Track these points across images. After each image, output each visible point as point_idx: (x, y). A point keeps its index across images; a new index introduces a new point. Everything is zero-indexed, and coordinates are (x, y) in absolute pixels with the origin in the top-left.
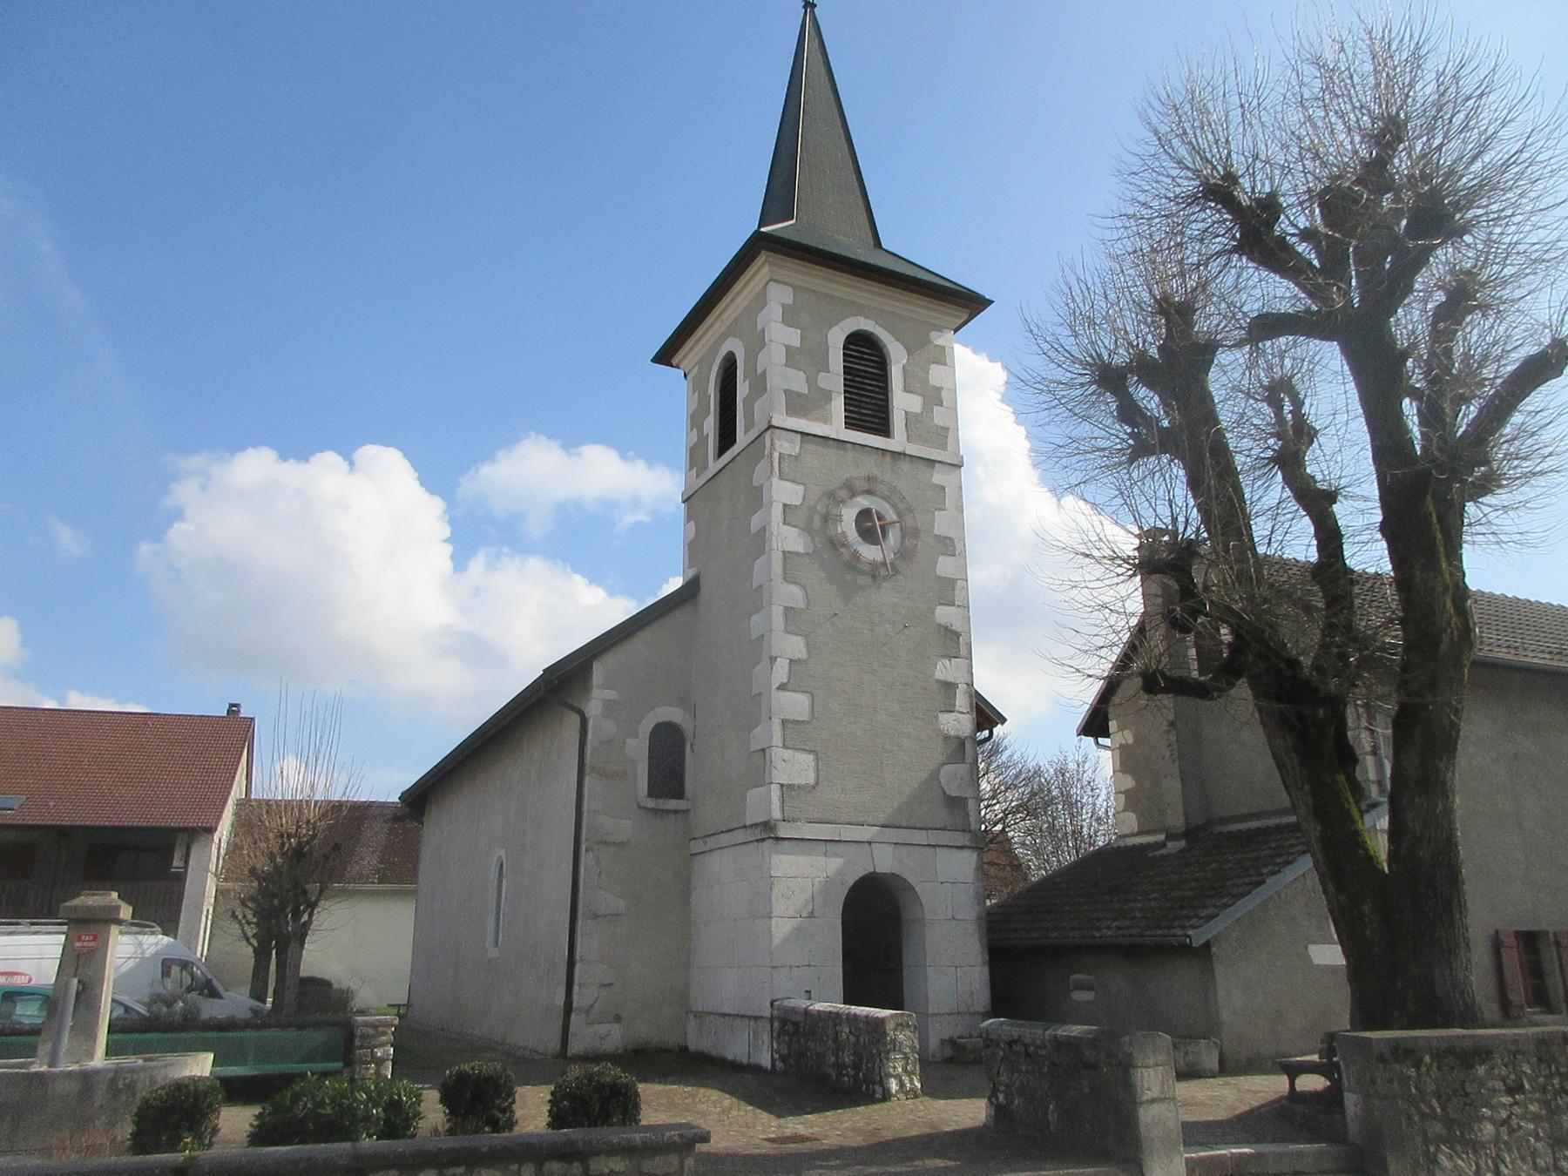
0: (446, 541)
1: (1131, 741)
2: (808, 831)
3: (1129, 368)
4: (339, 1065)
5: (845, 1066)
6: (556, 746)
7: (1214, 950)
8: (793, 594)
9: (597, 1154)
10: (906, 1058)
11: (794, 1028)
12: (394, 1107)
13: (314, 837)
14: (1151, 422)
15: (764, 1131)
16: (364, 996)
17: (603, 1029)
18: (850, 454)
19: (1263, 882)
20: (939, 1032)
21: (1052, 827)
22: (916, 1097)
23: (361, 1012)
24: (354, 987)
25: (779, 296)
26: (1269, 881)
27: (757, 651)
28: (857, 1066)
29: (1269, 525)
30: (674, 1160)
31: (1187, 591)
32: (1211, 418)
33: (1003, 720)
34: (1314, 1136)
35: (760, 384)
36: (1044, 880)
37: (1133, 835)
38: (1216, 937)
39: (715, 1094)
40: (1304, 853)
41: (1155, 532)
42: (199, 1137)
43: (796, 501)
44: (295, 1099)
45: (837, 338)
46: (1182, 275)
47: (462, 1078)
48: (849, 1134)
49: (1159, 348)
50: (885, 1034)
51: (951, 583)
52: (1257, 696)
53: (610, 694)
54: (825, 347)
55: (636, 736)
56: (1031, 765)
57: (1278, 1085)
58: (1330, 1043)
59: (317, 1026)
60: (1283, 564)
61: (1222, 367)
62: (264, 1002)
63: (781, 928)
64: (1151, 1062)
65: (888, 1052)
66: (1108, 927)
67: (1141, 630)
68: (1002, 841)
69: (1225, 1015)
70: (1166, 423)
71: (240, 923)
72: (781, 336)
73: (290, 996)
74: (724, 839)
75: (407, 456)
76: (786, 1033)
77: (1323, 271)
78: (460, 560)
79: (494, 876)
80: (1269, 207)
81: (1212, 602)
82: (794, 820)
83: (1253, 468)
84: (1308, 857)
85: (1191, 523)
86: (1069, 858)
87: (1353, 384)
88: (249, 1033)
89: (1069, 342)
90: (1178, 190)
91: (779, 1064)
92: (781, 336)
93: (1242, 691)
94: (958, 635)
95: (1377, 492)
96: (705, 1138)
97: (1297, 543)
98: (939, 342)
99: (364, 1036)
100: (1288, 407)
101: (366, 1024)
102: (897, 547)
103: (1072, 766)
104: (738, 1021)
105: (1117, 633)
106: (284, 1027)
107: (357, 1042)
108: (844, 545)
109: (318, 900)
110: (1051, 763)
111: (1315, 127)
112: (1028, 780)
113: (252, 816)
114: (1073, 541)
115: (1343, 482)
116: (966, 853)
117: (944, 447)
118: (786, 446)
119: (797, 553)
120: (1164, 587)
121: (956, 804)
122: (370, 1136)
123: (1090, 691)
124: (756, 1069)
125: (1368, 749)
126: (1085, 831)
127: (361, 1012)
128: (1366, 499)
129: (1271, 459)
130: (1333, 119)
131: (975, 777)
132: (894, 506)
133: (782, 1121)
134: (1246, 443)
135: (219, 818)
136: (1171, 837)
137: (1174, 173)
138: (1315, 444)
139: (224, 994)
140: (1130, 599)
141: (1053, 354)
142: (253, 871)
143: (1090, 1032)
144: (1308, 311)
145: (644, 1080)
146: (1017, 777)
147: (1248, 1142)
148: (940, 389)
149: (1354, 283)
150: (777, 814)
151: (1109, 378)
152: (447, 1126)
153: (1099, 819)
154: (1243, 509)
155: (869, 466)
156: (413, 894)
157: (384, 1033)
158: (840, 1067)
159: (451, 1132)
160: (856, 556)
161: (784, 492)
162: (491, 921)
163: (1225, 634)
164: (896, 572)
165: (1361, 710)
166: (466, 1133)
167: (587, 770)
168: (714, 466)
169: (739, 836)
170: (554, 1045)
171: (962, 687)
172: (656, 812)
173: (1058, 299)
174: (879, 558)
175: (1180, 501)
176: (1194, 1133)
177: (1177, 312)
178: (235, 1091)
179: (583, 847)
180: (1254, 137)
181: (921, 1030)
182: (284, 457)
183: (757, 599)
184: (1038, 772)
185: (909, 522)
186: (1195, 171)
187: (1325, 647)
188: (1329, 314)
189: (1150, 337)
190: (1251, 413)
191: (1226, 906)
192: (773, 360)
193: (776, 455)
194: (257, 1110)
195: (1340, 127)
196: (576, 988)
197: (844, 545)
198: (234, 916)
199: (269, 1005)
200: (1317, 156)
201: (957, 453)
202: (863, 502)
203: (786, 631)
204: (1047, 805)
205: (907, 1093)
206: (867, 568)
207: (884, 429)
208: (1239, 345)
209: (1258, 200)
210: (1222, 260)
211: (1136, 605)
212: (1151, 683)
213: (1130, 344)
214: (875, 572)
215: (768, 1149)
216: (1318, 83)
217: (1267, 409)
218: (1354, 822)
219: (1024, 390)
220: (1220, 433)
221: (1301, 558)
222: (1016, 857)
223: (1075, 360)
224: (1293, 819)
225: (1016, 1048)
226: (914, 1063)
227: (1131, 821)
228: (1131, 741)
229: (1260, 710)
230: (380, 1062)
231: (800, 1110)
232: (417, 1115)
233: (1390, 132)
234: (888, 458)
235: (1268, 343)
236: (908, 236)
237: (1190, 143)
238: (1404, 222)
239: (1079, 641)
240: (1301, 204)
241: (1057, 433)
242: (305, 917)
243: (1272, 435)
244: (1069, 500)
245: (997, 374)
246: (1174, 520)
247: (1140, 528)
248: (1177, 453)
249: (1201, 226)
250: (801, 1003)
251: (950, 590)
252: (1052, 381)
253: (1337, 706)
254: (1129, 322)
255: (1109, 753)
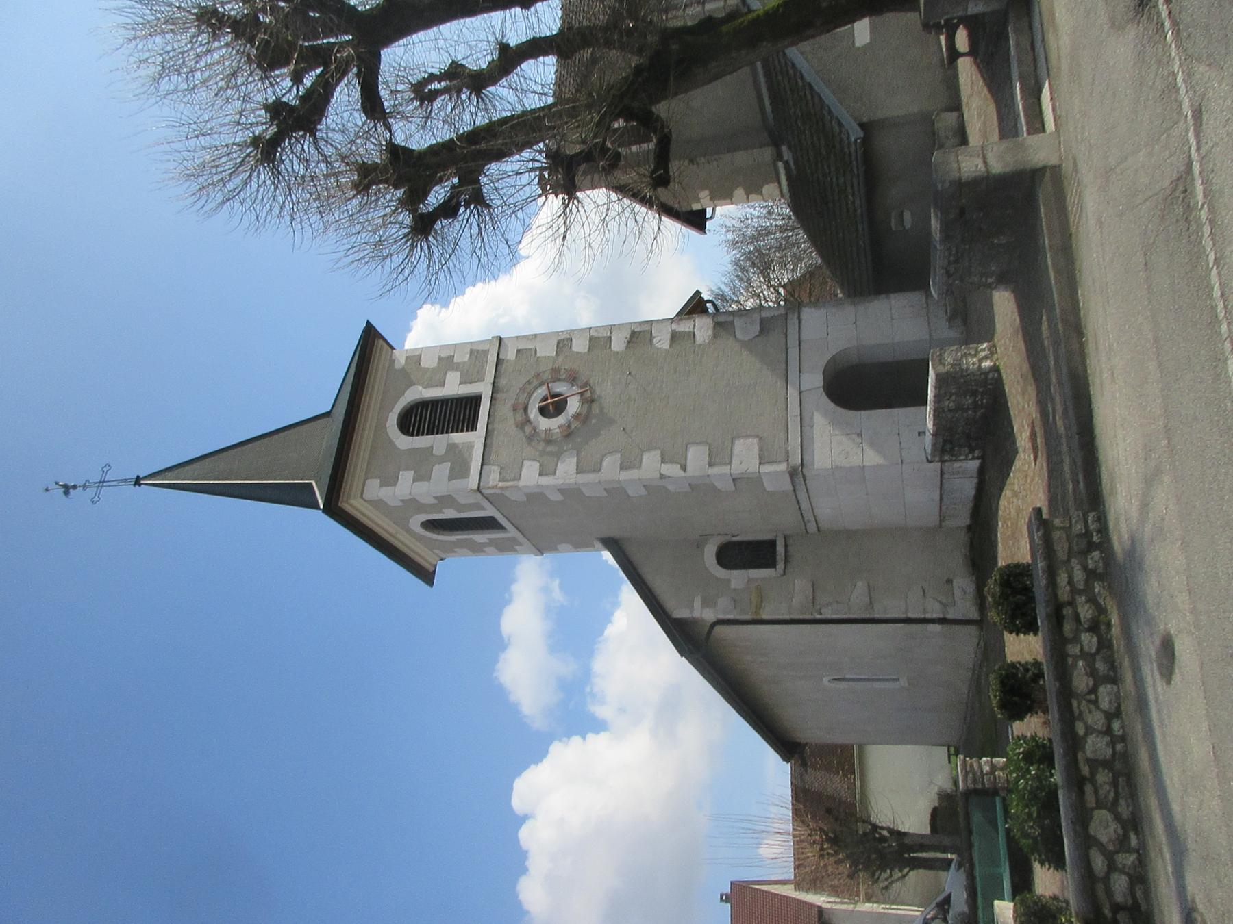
0: (584, 738)
1: (706, 192)
2: (795, 440)
3: (414, 211)
4: (998, 800)
5: (975, 402)
6: (741, 642)
7: (865, 120)
8: (610, 465)
9: (1055, 595)
10: (965, 355)
11: (948, 443)
12: (1029, 757)
13: (821, 830)
14: (455, 193)
15: (1029, 464)
16: (942, 781)
17: (958, 593)
18: (496, 426)
19: (810, 84)
20: (945, 331)
21: (779, 248)
22: (994, 346)
23: (956, 783)
24: (936, 790)
25: (374, 490)
26: (808, 78)
27: (656, 490)
28: (974, 393)
29: (531, 95)
30: (1056, 535)
31: (587, 157)
32: (448, 146)
33: (698, 293)
34: (1002, 37)
35: (446, 500)
36: (820, 253)
37: (783, 882)
38: (855, 119)
39: (1003, 503)
40: (784, 54)
41: (542, 182)
42: (1060, 911)
43: (536, 466)
44: (1026, 835)
45: (404, 442)
46: (336, 174)
47: (1003, 706)
48: (1026, 397)
49: (396, 188)
50: (947, 373)
51: (593, 340)
52: (666, 97)
53: (697, 602)
54: (413, 451)
55: (729, 581)
56: (730, 268)
57: (966, 67)
58: (930, 26)
59: (968, 816)
60: (560, 82)
61: (406, 139)
62: (952, 860)
63: (871, 458)
64: (955, 166)
65: (962, 370)
66: (853, 202)
67: (621, 189)
68: (792, 287)
69: (915, 108)
70: (456, 180)
71: (891, 883)
72: (406, 486)
73: (947, 841)
74: (805, 505)
75: (519, 774)
76: (952, 449)
77: (326, 65)
78: (599, 726)
79: (843, 685)
80: (276, 110)
81: (595, 136)
82: (787, 452)
83: (486, 110)
84: (788, 51)
85: (532, 157)
86: (802, 235)
87: (414, 36)
88: (977, 873)
89: (397, 260)
90: (268, 182)
91: (977, 453)
92: (406, 486)
93: (662, 109)
94: (633, 333)
95: (498, 13)
96: (1038, 511)
97: (542, 73)
98: (403, 361)
99: (975, 781)
100: (435, 86)
101: (965, 779)
102: (562, 385)
103: (730, 236)
104: (946, 487)
105: (624, 209)
106: (970, 846)
107: (979, 786)
108: (569, 426)
109: (870, 824)
110: (729, 253)
111: (210, 77)
112: (743, 270)
113: (807, 878)
114: (553, 248)
115: (491, 39)
116: (803, 316)
117: (486, 352)
118: (493, 477)
119: (578, 463)
120: (585, 173)
121: (766, 326)
122: (1052, 775)
123: (671, 226)
124: (981, 471)
125: (699, 8)
126: (779, 223)
127: (956, 783)
128: (504, 20)
129: (478, 96)
130: (202, 64)
131: (742, 313)
132: (536, 388)
133: (1020, 450)
134: (467, 116)
135: (811, 905)
136: (779, 156)
137: (255, 186)
138: (464, 62)
139: (947, 893)
140: (595, 198)
141: (406, 272)
142: (851, 876)
143: (936, 215)
144: (358, 75)
145: (995, 559)
146: (741, 279)
147: (1012, 87)
148: (440, 359)
149: (332, 40)
150: (783, 467)
151: (423, 227)
152: (1040, 714)
153: (769, 213)
154: (519, 116)
155: (505, 410)
156: (861, 747)
157: (972, 766)
158: (976, 406)
159: (1046, 711)
160: (577, 416)
161: (530, 475)
162: (877, 685)
163: (619, 123)
164: (587, 384)
165: (670, 16)
166: (1046, 700)
167: (758, 617)
168: (512, 532)
169: (802, 496)
170: (973, 630)
171: (674, 326)
172: (787, 560)
173: (361, 272)
174: (577, 398)
175: (516, 167)
176: (1008, 128)
177: (366, 177)
178: (1022, 884)
179: (818, 617)
180: (221, 126)
181: (943, 345)
182: (524, 870)
183: (616, 492)
184: (736, 263)
185: (547, 376)
186: (252, 171)
187: (622, 47)
188: (359, 57)
189: (388, 197)
190: (442, 113)
191: (830, 112)
192: (425, 491)
193: (501, 484)
194: (1036, 866)
195: (209, 59)
196: (928, 616)
197: (569, 426)
198: (887, 888)
199: (954, 856)
200: (234, 75)
201: (490, 342)
202: (533, 413)
203: (640, 467)
204: (761, 254)
205: (992, 353)
206: (586, 406)
207: (475, 400)
208: (388, 128)
209: (272, 120)
210: (322, 144)
211: (600, 195)
212: (662, 180)
213: (394, 212)
214: (588, 400)
215: (1042, 459)
216: (175, 78)
217: (438, 103)
218: (758, 16)
219: (439, 290)
220: (460, 137)
221: (553, 69)
222: (803, 276)
223: (410, 255)
224: (759, 64)
225: (952, 270)
226: (969, 349)
227: (770, 188)
228: (706, 192)
229: (676, 94)
230: (994, 768)
231: (1010, 436)
232: (1033, 738)
233: (209, 19)
234: (499, 396)
235: (386, 104)
236: (321, 391)
237: (230, 175)
238: (282, 4)
239: (632, 239)
240: (272, 85)
241: (469, 265)
242: (885, 833)
243: (458, 96)
244: (523, 249)
245: (427, 313)
246: (532, 170)
247: (540, 196)
248: (479, 170)
249: (296, 163)
250: (928, 439)
251: (599, 341)
252: (428, 271)
253: (671, 35)
254: (376, 215)
255: (718, 209)
